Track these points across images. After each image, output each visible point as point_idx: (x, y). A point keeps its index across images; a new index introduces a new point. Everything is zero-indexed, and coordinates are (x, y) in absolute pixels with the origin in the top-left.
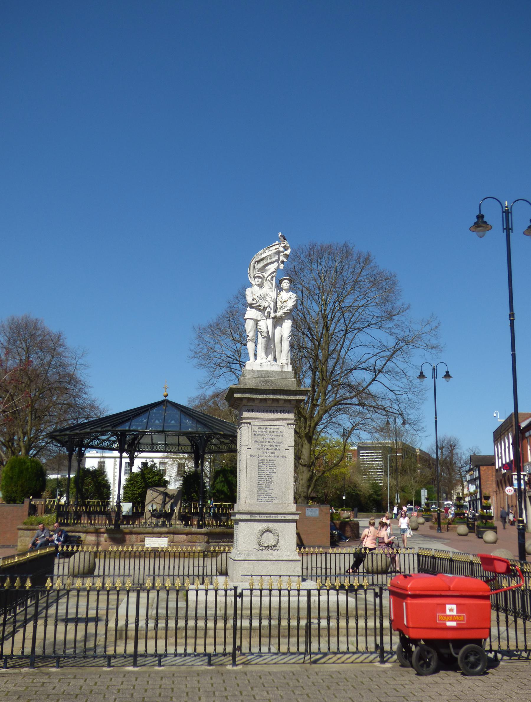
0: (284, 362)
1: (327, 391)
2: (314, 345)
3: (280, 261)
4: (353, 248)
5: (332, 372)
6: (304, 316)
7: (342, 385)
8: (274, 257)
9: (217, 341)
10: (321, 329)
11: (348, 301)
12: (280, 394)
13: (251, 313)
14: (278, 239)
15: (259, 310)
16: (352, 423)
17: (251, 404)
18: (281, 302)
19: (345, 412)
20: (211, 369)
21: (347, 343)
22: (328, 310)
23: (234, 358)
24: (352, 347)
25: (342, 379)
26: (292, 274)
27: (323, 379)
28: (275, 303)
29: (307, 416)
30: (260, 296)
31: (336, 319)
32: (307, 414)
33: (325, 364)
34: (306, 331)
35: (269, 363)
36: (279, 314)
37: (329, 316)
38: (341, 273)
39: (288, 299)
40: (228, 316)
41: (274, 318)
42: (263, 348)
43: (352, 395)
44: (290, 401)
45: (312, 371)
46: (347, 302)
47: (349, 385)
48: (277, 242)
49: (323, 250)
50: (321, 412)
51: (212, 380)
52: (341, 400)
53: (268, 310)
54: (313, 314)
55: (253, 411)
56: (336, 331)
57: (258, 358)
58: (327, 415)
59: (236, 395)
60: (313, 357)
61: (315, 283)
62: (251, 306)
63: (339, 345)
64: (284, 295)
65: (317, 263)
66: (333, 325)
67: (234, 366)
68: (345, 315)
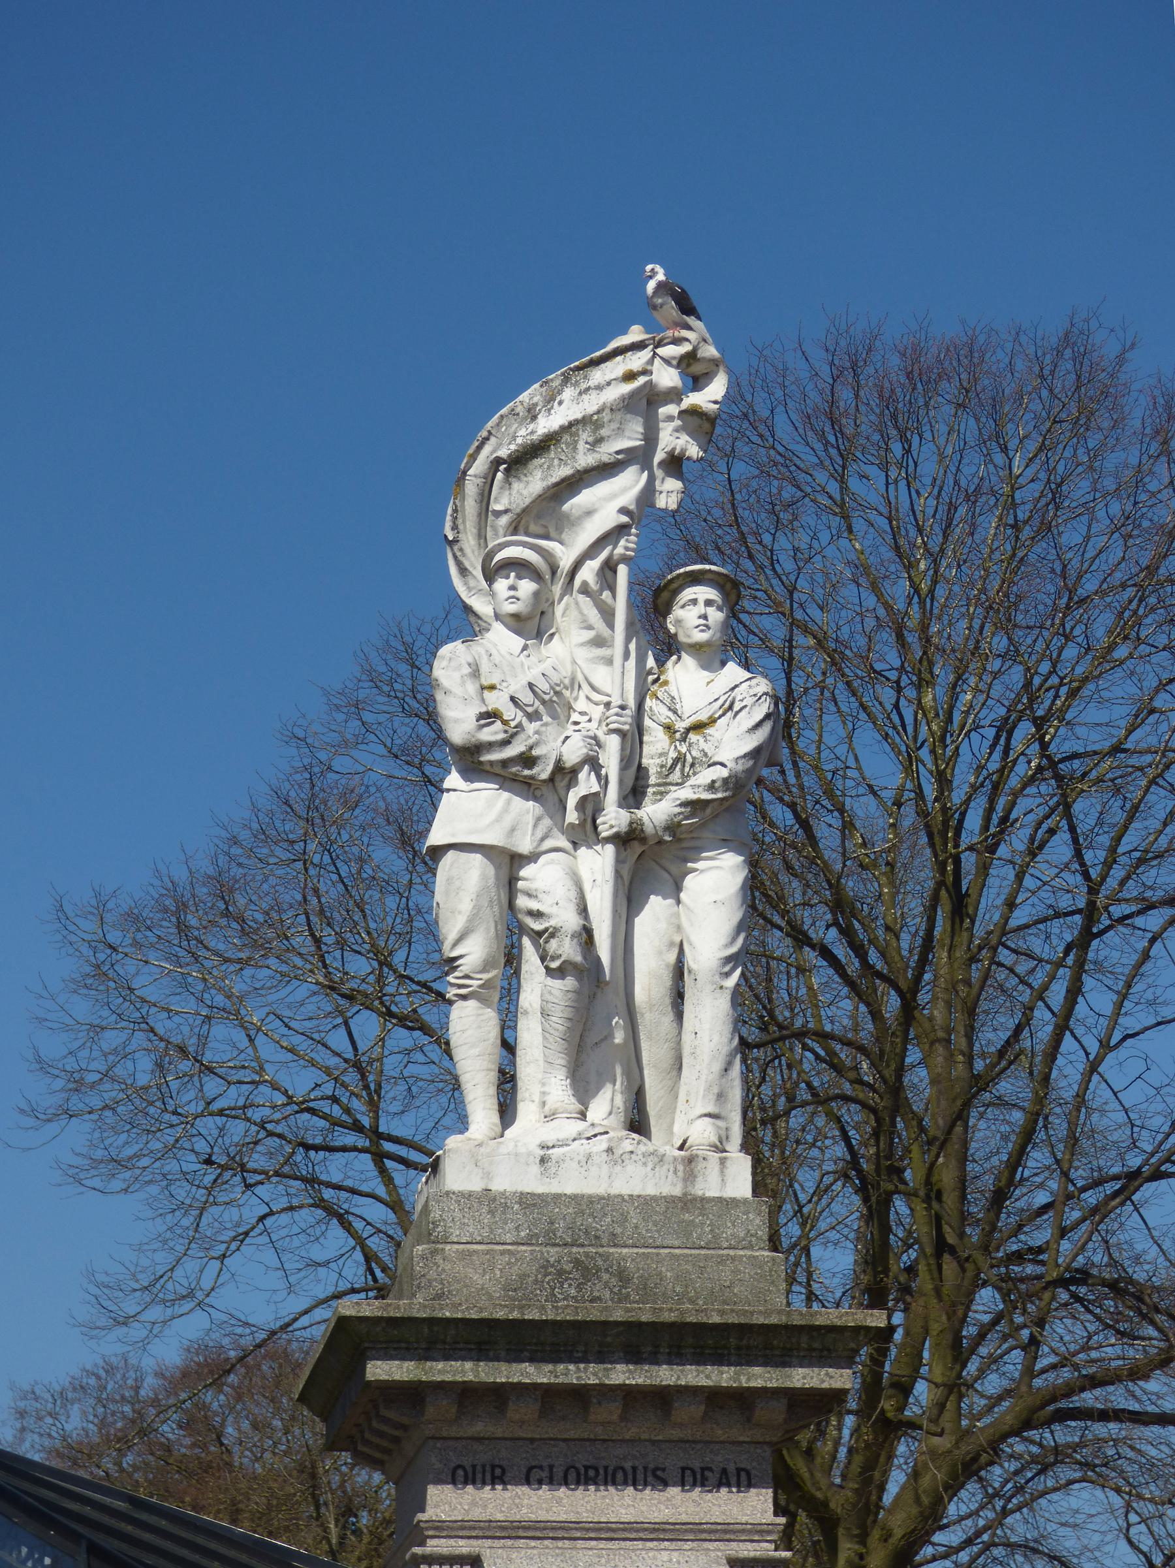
0: (702, 1133)
1: (970, 1331)
2: (876, 1015)
3: (659, 456)
4: (1121, 359)
5: (999, 1197)
6: (805, 825)
7: (1063, 1282)
8: (620, 431)
9: (220, 1000)
10: (915, 906)
11: (1102, 716)
12: (676, 1356)
13: (468, 812)
14: (646, 312)
15: (527, 788)
16: (1146, 1543)
17: (479, 1428)
18: (669, 728)
19: (1095, 1471)
20: (181, 1191)
21: (1097, 998)
22: (963, 778)
23: (336, 1111)
24: (1129, 1023)
25: (1065, 1245)
26: (720, 546)
27: (941, 1247)
28: (633, 738)
29: (838, 1503)
30: (527, 697)
31: (1018, 840)
32: (834, 1483)
33: (954, 1146)
34: (819, 923)
35: (601, 1143)
36: (656, 812)
37: (973, 821)
38: (1046, 528)
39: (718, 710)
40: (294, 828)
41: (628, 839)
42: (557, 1045)
43: (1134, 1353)
44: (741, 1401)
45: (863, 1190)
46: (1091, 725)
47: (1119, 1287)
48: (636, 334)
49: (921, 375)
50: (937, 1475)
51: (190, 1266)
52: (1070, 1390)
53: (587, 784)
54: (863, 808)
55: (494, 1475)
56: (1019, 917)
57: (527, 1111)
58: (968, 1498)
59: (379, 1370)
60: (872, 1098)
61: (871, 601)
62: (472, 761)
63: (1041, 1013)
64: (691, 685)
65: (885, 467)
66: (1001, 878)
67: (334, 1168)
68: (1078, 807)
